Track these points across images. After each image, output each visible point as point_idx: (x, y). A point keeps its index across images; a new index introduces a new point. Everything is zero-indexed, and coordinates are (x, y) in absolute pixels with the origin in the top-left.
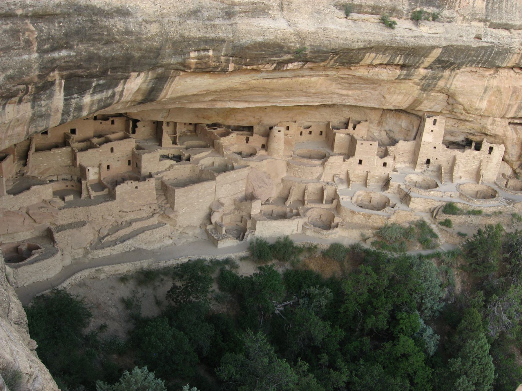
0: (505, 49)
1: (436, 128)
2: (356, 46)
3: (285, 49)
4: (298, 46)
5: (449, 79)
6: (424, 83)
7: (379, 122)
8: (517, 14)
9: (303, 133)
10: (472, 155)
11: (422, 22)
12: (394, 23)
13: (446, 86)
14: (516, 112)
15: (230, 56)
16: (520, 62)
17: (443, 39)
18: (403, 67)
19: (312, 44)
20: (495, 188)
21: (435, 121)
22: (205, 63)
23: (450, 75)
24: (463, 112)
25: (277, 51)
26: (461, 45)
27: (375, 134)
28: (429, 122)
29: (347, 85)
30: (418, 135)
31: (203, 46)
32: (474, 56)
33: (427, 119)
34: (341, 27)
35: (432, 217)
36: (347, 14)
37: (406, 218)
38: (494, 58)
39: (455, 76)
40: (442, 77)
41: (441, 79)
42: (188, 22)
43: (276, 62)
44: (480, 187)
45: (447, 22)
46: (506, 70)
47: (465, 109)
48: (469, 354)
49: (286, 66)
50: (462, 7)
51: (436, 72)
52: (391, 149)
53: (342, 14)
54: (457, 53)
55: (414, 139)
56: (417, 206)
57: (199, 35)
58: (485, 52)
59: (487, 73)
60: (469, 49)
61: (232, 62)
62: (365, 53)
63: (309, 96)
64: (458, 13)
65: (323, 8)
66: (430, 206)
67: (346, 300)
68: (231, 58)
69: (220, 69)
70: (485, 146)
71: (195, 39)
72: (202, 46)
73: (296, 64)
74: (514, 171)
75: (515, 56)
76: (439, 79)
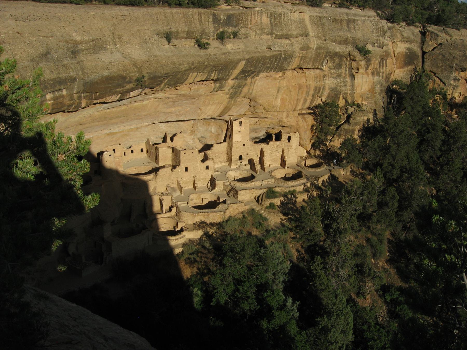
0: (289, 55)
1: (242, 129)
2: (183, 68)
3: (128, 79)
4: (137, 75)
5: (250, 85)
6: (232, 92)
7: (192, 131)
8: (293, 25)
9: (126, 153)
10: (275, 146)
11: (227, 40)
12: (208, 44)
13: (249, 92)
14: (303, 105)
15: (82, 93)
16: (300, 63)
17: (245, 53)
18: (215, 81)
19: (149, 71)
20: (299, 169)
21: (241, 123)
22: (61, 103)
23: (251, 82)
24: (263, 111)
25: (121, 82)
26: (258, 56)
27: (189, 143)
28: (236, 125)
29: (171, 103)
30: (228, 136)
31: (58, 86)
32: (268, 64)
33: (234, 122)
34: (166, 53)
35: (259, 204)
36: (169, 41)
37: (238, 209)
38: (282, 63)
39: (255, 82)
40: (245, 84)
41: (245, 87)
42: (41, 65)
43: (121, 92)
44: (290, 172)
45: (244, 38)
46: (291, 71)
47: (264, 109)
48: (332, 310)
49: (128, 95)
50: (253, 24)
51: (241, 81)
52: (209, 152)
53: (164, 41)
54: (256, 63)
55: (225, 140)
56: (244, 197)
57: (53, 76)
58: (276, 59)
59: (277, 76)
60: (264, 58)
61: (84, 98)
62: (189, 74)
63: (140, 119)
64: (251, 29)
65: (148, 38)
66: (254, 195)
67: (216, 293)
68: (83, 95)
69: (73, 106)
70: (284, 137)
71: (50, 80)
72: (58, 87)
73: (136, 91)
74: (308, 152)
75: (297, 59)
76: (243, 87)
